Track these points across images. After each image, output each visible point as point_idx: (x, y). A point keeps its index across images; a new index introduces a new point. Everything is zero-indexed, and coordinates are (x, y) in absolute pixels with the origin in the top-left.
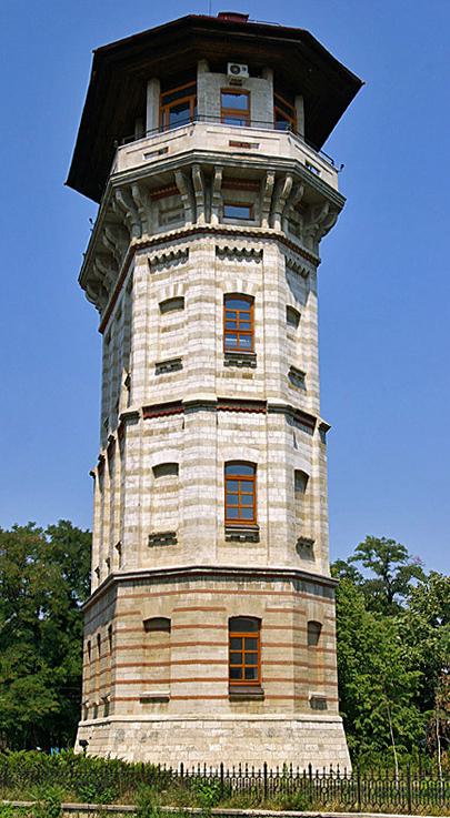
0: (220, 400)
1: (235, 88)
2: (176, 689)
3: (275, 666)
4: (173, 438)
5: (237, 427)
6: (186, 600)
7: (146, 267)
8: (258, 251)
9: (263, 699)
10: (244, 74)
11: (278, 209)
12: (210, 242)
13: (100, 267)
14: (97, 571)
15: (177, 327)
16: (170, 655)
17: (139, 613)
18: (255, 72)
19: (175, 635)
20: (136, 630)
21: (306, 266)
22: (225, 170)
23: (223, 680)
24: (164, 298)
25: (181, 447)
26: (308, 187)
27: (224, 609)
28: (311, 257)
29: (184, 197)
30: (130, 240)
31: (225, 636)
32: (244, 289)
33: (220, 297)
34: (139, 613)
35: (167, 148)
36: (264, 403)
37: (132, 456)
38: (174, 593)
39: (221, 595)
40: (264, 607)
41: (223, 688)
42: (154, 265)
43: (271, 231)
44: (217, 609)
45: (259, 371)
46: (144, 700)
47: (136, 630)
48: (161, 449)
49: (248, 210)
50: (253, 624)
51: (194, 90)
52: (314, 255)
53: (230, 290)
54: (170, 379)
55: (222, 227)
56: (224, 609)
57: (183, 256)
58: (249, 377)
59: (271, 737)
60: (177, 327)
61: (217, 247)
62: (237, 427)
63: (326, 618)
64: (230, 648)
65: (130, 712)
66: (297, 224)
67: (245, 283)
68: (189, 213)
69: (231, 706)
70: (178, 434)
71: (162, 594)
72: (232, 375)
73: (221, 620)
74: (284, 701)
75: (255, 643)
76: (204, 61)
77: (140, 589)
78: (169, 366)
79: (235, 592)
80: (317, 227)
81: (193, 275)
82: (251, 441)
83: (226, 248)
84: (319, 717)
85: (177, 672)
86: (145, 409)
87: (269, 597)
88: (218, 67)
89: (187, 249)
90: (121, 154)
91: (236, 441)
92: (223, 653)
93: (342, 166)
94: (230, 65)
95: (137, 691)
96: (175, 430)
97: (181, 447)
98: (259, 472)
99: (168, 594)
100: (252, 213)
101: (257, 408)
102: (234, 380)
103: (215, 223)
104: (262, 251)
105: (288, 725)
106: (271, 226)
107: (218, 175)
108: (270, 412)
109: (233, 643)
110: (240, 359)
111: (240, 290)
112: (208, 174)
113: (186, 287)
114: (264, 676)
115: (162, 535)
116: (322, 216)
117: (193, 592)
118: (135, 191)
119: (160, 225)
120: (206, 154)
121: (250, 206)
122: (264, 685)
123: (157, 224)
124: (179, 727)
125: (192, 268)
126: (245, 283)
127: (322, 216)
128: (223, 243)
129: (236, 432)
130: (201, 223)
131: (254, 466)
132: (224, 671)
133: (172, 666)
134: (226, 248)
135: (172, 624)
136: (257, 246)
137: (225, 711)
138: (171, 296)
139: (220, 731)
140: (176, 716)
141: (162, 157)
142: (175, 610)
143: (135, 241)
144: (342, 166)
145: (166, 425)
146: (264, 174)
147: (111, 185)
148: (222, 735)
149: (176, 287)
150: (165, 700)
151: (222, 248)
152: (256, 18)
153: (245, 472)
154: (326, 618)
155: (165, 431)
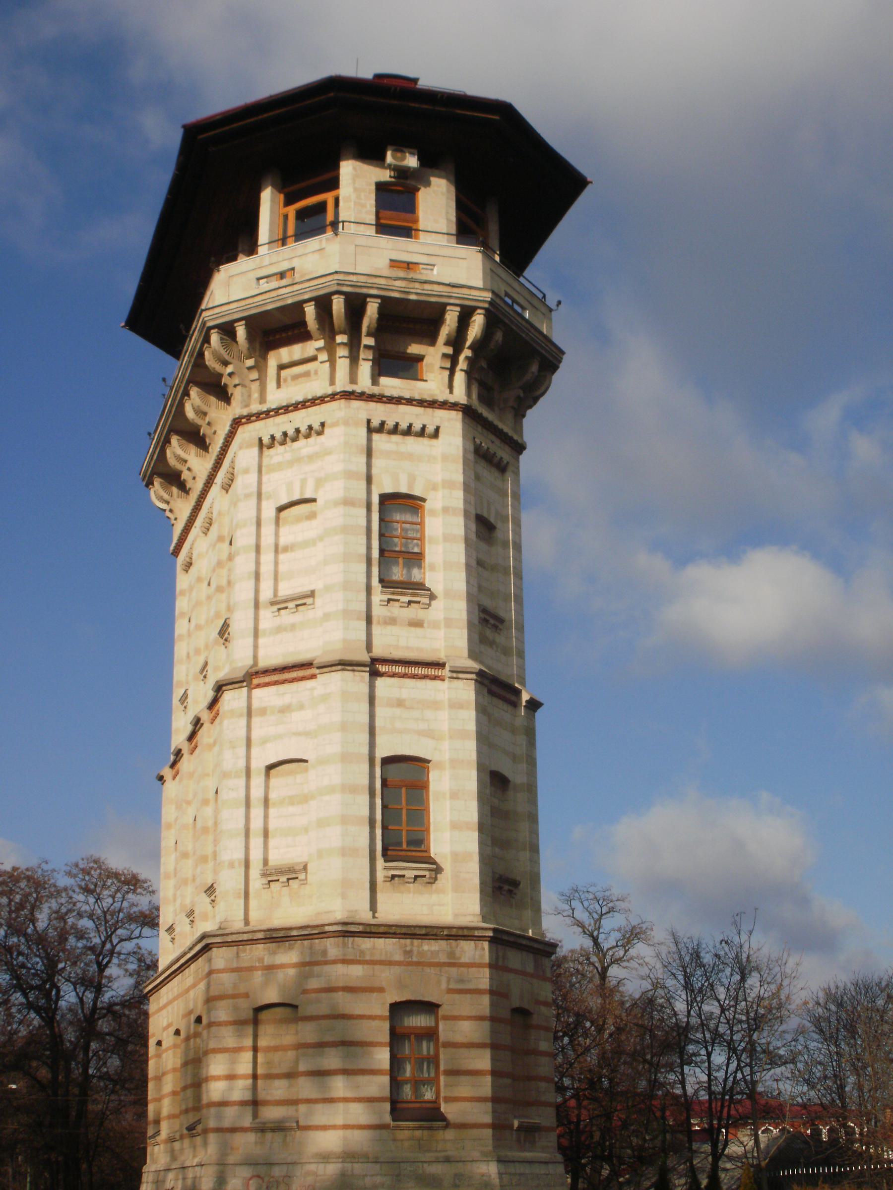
8: (430, 429)
11: (462, 364)
13: (179, 452)
14: (171, 929)
21: (503, 453)
24: (284, 501)
25: (307, 734)
27: (381, 990)
28: (511, 438)
32: (410, 486)
35: (293, 269)
36: (308, 665)
40: (444, 986)
43: (452, 399)
51: (333, 184)
52: (515, 437)
53: (389, 490)
54: (293, 627)
55: (376, 390)
56: (381, 990)
58: (417, 624)
61: (369, 421)
63: (538, 1002)
67: (412, 479)
70: (307, 714)
72: (392, 621)
74: (475, 1132)
76: (191, 385)
78: (291, 605)
80: (522, 395)
82: (422, 726)
84: (528, 1155)
87: (453, 971)
89: (323, 425)
91: (398, 725)
93: (559, 303)
96: (301, 707)
101: (432, 672)
104: (437, 429)
107: (372, 309)
111: (404, 490)
113: (319, 483)
115: (281, 871)
116: (528, 377)
118: (241, 331)
120: (354, 278)
126: (412, 479)
127: (528, 377)
128: (379, 412)
129: (398, 711)
134: (383, 424)
138: (296, 497)
141: (284, 282)
144: (559, 303)
145: (287, 699)
146: (440, 310)
147: (204, 323)
149: (303, 482)
153: (392, 218)
155: (285, 710)
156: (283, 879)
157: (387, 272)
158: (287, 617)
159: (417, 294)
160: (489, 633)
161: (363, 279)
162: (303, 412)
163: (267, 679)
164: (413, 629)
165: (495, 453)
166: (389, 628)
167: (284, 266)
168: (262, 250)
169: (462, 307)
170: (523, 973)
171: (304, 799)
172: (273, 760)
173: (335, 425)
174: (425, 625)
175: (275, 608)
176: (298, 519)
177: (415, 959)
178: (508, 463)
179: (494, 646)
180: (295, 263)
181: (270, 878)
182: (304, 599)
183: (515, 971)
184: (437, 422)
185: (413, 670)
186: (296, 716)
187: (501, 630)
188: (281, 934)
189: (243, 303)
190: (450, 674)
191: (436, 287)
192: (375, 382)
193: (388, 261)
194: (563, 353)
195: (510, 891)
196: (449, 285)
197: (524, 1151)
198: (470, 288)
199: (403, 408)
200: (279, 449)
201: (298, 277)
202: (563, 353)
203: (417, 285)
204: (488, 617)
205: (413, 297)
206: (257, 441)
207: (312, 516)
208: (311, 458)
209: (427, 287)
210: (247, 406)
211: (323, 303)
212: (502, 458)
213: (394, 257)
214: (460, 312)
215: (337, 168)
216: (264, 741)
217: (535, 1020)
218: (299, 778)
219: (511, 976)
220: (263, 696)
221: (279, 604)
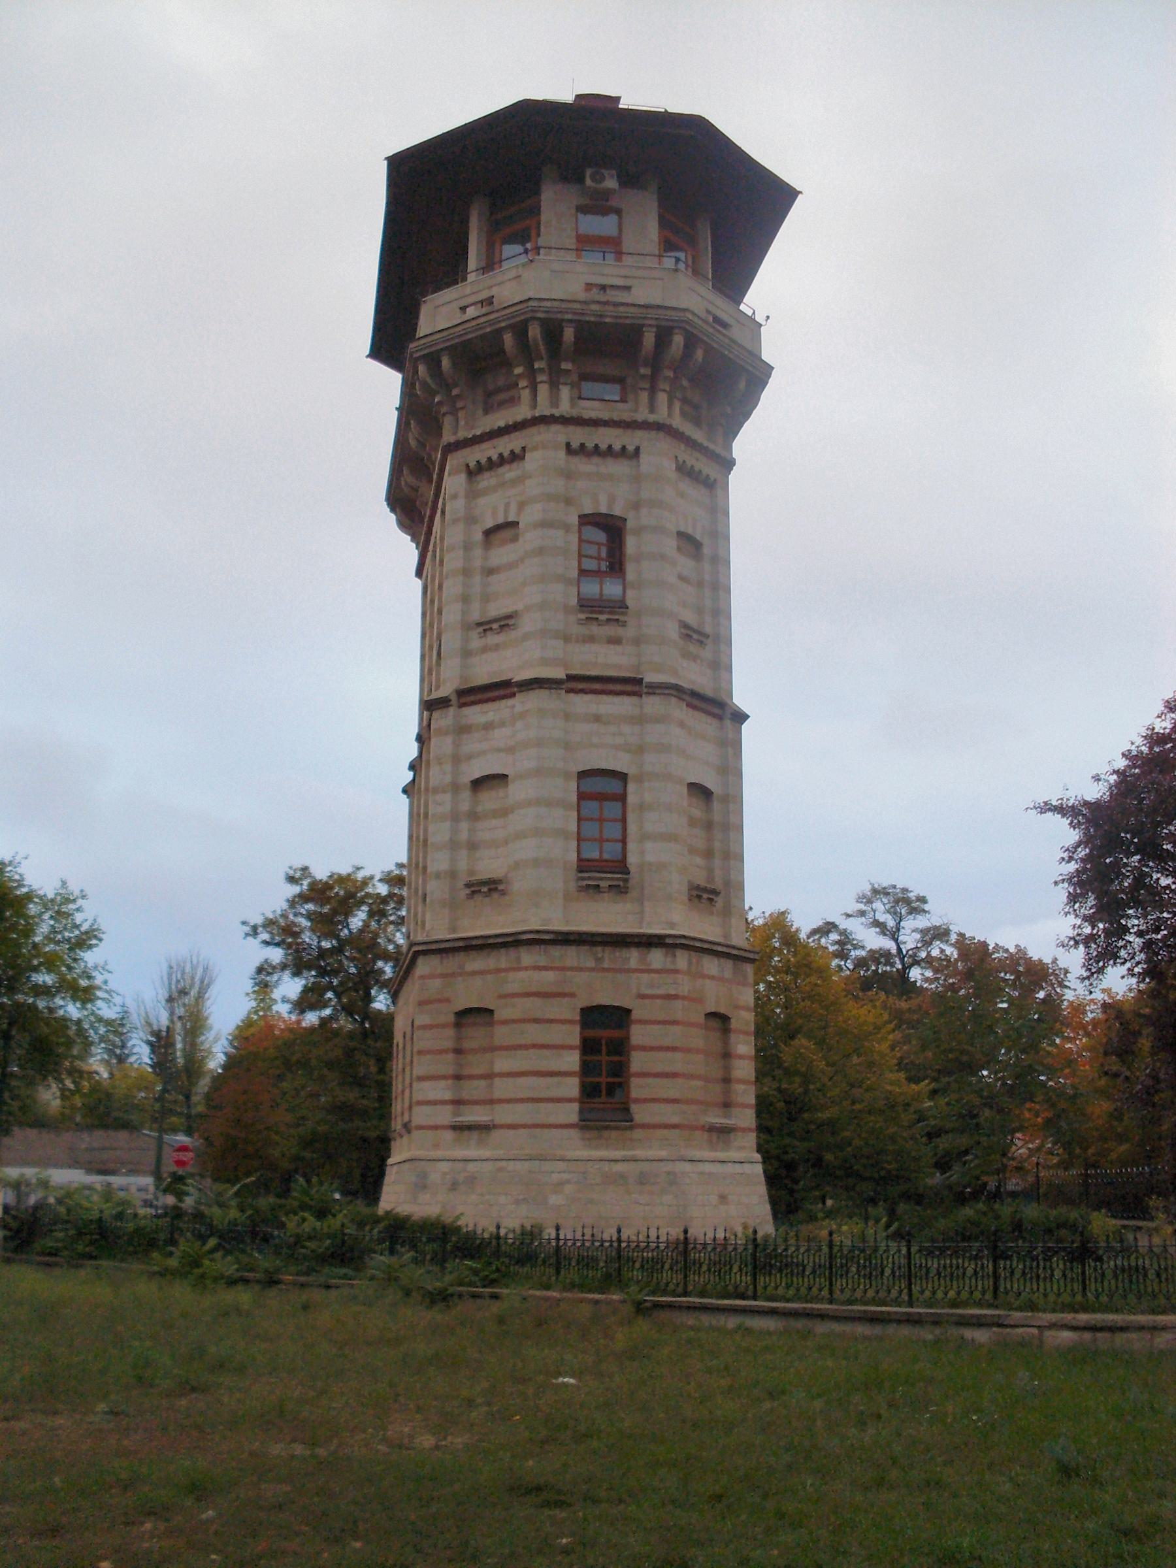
0: (571, 678)
1: (598, 205)
2: (503, 1114)
3: (650, 1080)
4: (500, 736)
5: (597, 718)
6: (517, 981)
7: (463, 477)
8: (631, 448)
9: (631, 1128)
10: (611, 183)
12: (558, 434)
15: (510, 566)
16: (492, 1063)
17: (448, 1000)
18: (629, 181)
19: (502, 1034)
20: (443, 1026)
22: (582, 327)
23: (570, 1100)
24: (490, 524)
25: (510, 750)
26: (709, 350)
29: (518, 370)
30: (440, 435)
31: (573, 1035)
32: (610, 506)
33: (575, 520)
34: (448, 1000)
36: (507, 684)
37: (440, 764)
38: (498, 971)
39: (569, 973)
40: (634, 991)
41: (570, 1113)
42: (474, 472)
43: (652, 418)
44: (563, 995)
45: (629, 632)
46: (458, 1128)
47: (443, 1026)
48: (483, 753)
49: (618, 387)
50: (619, 1017)
51: (535, 211)
54: (497, 647)
55: (575, 413)
57: (516, 457)
58: (615, 641)
59: (642, 1183)
60: (510, 566)
61: (568, 445)
62: (597, 718)
63: (737, 1007)
64: (583, 1028)
65: (436, 1146)
66: (696, 407)
67: (612, 500)
68: (526, 394)
69: (583, 1139)
70: (506, 731)
71: (482, 973)
72: (591, 639)
73: (569, 1010)
75: (620, 1048)
77: (451, 963)
78: (495, 626)
79: (592, 970)
81: (532, 487)
82: (620, 740)
83: (582, 445)
84: (720, 1155)
85: (502, 1088)
86: (461, 693)
87: (645, 976)
88: (572, 175)
89: (524, 449)
90: (425, 312)
91: (595, 740)
92: (572, 1060)
93: (768, 317)
94: (588, 172)
95: (445, 1115)
96: (502, 724)
97: (510, 750)
98: (631, 787)
99: (489, 972)
100: (624, 391)
101: (629, 688)
102: (595, 647)
103: (565, 407)
104: (637, 449)
105: (669, 1167)
106: (652, 410)
107: (569, 334)
108: (649, 694)
109: (588, 1047)
110: (601, 613)
111: (603, 510)
112: (552, 330)
114: (634, 1094)
117: (526, 969)
118: (446, 362)
119: (486, 411)
120: (548, 304)
121: (621, 381)
122: (634, 1108)
123: (480, 412)
124: (501, 1169)
125: (530, 477)
126: (612, 500)
128: (578, 435)
129: (595, 726)
130: (544, 408)
131: (622, 777)
132: (572, 1087)
133: (497, 1081)
134: (582, 445)
135: (497, 1016)
136: (630, 439)
137: (574, 1146)
138: (501, 520)
139: (565, 1176)
140: (500, 1153)
142: (501, 997)
143: (448, 437)
148: (568, 1182)
149: (507, 505)
150: (484, 1128)
151: (472, 464)
152: (633, 99)
154: (737, 1007)
156: (485, 889)
157: (582, 296)
158: (492, 639)
159: (611, 317)
160: (693, 648)
161: (556, 304)
162: (506, 439)
163: (472, 698)
164: (612, 647)
165: (700, 471)
166: (587, 645)
167: (485, 295)
168: (471, 277)
169: (658, 327)
170: (721, 979)
171: (504, 812)
172: (477, 775)
173: (535, 448)
174: (624, 641)
175: (481, 629)
176: (504, 542)
177: (606, 965)
178: (715, 480)
179: (699, 661)
180: (494, 291)
181: (473, 889)
182: (505, 622)
183: (712, 978)
184: (637, 442)
185: (611, 687)
186: (497, 733)
187: (706, 645)
188: (479, 942)
189: (445, 333)
190: (645, 690)
191: (632, 310)
192: (573, 405)
193: (583, 285)
194: (773, 368)
195: (711, 900)
196: (643, 306)
197: (716, 1151)
198: (666, 308)
199: (602, 430)
200: (487, 475)
201: (496, 305)
202: (773, 368)
203: (611, 308)
204: (689, 632)
205: (608, 320)
206: (464, 468)
207: (515, 539)
208: (515, 482)
209: (621, 309)
210: (455, 433)
211: (520, 330)
212: (708, 475)
213: (589, 281)
214: (656, 333)
215: (537, 192)
216: (470, 757)
217: (734, 1024)
218: (501, 793)
219: (707, 981)
220: (476, 714)
221: (485, 626)
